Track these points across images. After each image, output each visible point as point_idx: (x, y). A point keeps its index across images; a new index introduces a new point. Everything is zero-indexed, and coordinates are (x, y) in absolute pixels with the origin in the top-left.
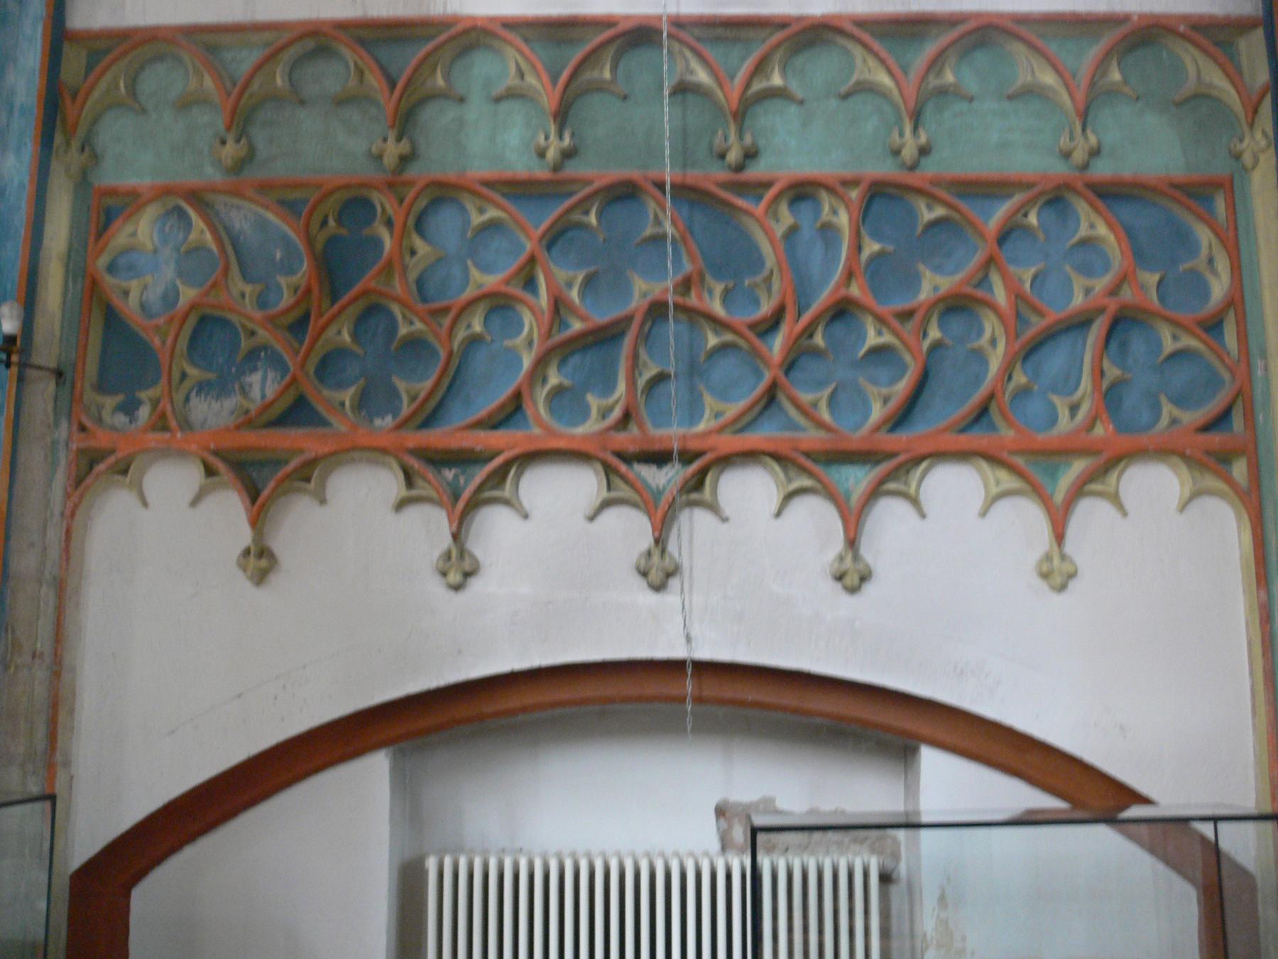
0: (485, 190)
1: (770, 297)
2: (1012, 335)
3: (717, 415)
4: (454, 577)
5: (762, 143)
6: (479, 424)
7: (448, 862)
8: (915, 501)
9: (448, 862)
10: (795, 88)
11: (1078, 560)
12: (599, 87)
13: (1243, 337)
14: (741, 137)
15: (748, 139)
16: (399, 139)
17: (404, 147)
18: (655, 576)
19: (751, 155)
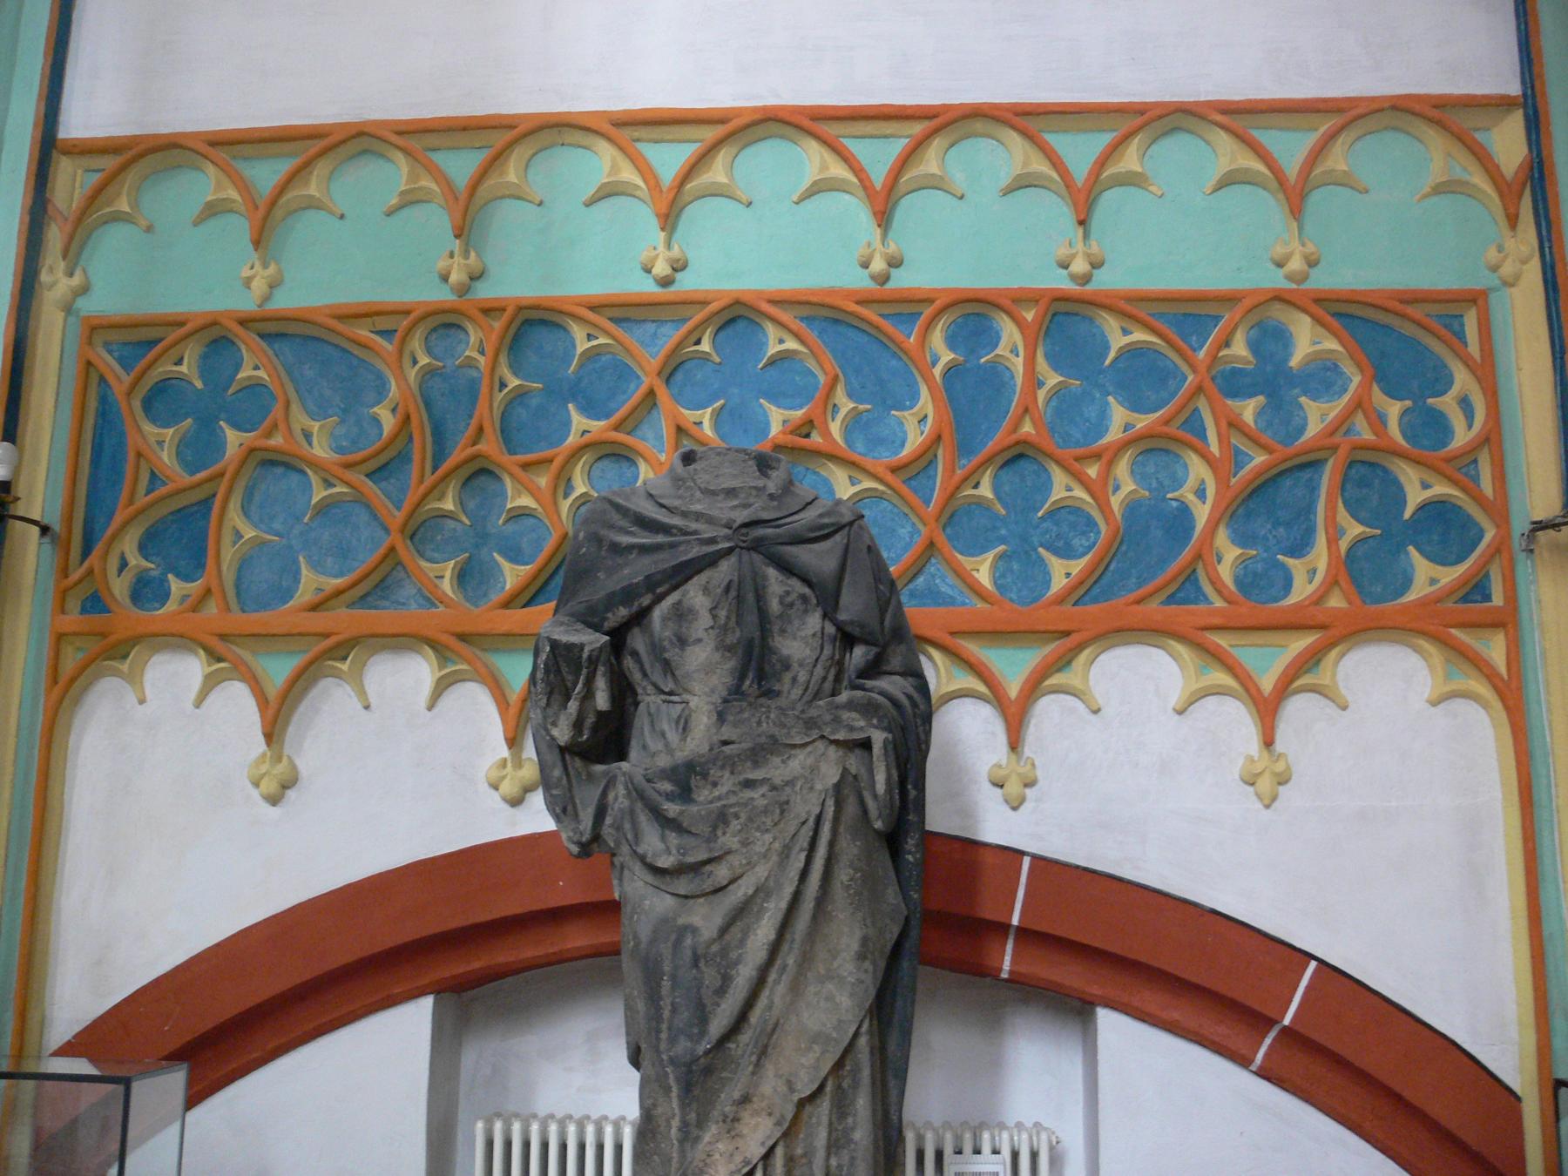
0: (591, 316)
1: (1470, 427)
2: (1222, 482)
3: (1433, 581)
4: (1265, 784)
5: (690, 256)
6: (507, 604)
7: (516, 1128)
8: (362, 693)
9: (516, 1128)
10: (959, 178)
11: (301, 764)
12: (313, 205)
13: (1500, 477)
14: (669, 246)
15: (676, 252)
16: (265, 266)
17: (77, 280)
18: (269, 786)
19: (476, 277)
